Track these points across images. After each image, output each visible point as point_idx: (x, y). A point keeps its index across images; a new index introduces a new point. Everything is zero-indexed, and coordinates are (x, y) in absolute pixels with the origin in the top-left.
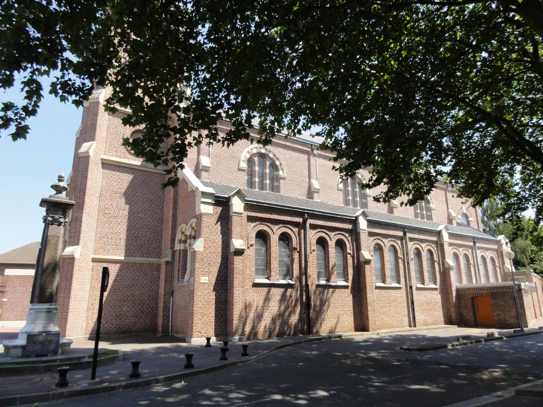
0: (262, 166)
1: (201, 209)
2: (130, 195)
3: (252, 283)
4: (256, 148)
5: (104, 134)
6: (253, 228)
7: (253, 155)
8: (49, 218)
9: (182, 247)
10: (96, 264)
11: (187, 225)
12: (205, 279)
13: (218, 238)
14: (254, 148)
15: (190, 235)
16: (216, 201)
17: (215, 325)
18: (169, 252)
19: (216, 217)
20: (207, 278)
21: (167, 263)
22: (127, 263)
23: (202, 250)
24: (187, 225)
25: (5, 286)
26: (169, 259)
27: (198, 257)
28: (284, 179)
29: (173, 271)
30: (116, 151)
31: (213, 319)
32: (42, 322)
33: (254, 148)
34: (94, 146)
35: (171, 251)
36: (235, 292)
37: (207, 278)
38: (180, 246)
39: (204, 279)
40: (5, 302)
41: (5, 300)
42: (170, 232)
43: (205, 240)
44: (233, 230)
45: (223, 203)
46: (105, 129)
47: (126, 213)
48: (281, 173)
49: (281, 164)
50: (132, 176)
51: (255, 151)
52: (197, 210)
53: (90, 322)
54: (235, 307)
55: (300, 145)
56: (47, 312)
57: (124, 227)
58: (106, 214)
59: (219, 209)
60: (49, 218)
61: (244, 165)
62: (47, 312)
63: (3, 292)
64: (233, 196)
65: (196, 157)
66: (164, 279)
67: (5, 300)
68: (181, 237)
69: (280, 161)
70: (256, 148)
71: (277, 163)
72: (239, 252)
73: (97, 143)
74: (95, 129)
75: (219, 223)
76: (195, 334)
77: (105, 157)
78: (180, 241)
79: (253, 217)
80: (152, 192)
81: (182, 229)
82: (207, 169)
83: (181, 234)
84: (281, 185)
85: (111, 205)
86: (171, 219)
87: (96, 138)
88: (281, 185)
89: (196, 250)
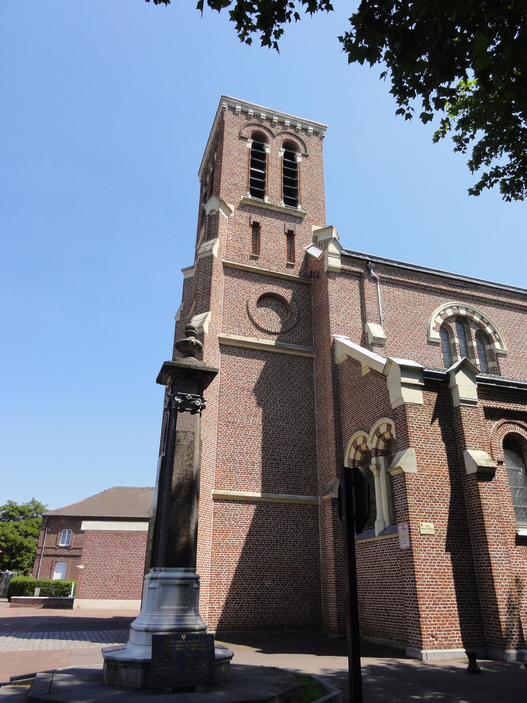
0: (465, 336)
1: (404, 395)
2: (263, 392)
3: (513, 536)
4: (451, 307)
5: (221, 302)
6: (497, 431)
7: (448, 319)
8: (177, 399)
10: (219, 505)
11: (368, 433)
12: (429, 526)
13: (440, 448)
14: (447, 308)
15: (376, 450)
16: (425, 381)
17: (461, 624)
19: (430, 410)
20: (432, 525)
22: (265, 503)
23: (416, 471)
24: (368, 433)
25: (81, 549)
27: (411, 485)
28: (504, 355)
30: (239, 326)
31: (455, 610)
32: (173, 607)
33: (447, 308)
34: (209, 319)
36: (492, 554)
39: (427, 527)
40: (82, 570)
41: (81, 567)
42: (332, 448)
43: (418, 453)
44: (467, 434)
45: (438, 385)
46: (221, 294)
47: (259, 420)
48: (497, 345)
49: (495, 332)
50: (263, 363)
51: (450, 313)
52: (392, 400)
53: (216, 606)
54: (497, 585)
55: (521, 299)
56: (180, 585)
57: (258, 443)
58: (229, 422)
59: (433, 396)
60: (177, 399)
61: (435, 335)
62: (180, 585)
63: (79, 556)
64: (456, 371)
65: (360, 325)
67: (81, 567)
68: (378, 444)
69: (492, 328)
70: (451, 307)
71: (489, 330)
72: (486, 474)
73: (212, 315)
74: (209, 294)
75: (437, 422)
76: (427, 640)
77: (223, 335)
79: (493, 409)
80: (294, 387)
81: (355, 441)
82: (382, 342)
83: (353, 450)
84: (501, 366)
85: (236, 408)
86: (331, 427)
87: (212, 306)
88: (501, 365)
89: (405, 470)
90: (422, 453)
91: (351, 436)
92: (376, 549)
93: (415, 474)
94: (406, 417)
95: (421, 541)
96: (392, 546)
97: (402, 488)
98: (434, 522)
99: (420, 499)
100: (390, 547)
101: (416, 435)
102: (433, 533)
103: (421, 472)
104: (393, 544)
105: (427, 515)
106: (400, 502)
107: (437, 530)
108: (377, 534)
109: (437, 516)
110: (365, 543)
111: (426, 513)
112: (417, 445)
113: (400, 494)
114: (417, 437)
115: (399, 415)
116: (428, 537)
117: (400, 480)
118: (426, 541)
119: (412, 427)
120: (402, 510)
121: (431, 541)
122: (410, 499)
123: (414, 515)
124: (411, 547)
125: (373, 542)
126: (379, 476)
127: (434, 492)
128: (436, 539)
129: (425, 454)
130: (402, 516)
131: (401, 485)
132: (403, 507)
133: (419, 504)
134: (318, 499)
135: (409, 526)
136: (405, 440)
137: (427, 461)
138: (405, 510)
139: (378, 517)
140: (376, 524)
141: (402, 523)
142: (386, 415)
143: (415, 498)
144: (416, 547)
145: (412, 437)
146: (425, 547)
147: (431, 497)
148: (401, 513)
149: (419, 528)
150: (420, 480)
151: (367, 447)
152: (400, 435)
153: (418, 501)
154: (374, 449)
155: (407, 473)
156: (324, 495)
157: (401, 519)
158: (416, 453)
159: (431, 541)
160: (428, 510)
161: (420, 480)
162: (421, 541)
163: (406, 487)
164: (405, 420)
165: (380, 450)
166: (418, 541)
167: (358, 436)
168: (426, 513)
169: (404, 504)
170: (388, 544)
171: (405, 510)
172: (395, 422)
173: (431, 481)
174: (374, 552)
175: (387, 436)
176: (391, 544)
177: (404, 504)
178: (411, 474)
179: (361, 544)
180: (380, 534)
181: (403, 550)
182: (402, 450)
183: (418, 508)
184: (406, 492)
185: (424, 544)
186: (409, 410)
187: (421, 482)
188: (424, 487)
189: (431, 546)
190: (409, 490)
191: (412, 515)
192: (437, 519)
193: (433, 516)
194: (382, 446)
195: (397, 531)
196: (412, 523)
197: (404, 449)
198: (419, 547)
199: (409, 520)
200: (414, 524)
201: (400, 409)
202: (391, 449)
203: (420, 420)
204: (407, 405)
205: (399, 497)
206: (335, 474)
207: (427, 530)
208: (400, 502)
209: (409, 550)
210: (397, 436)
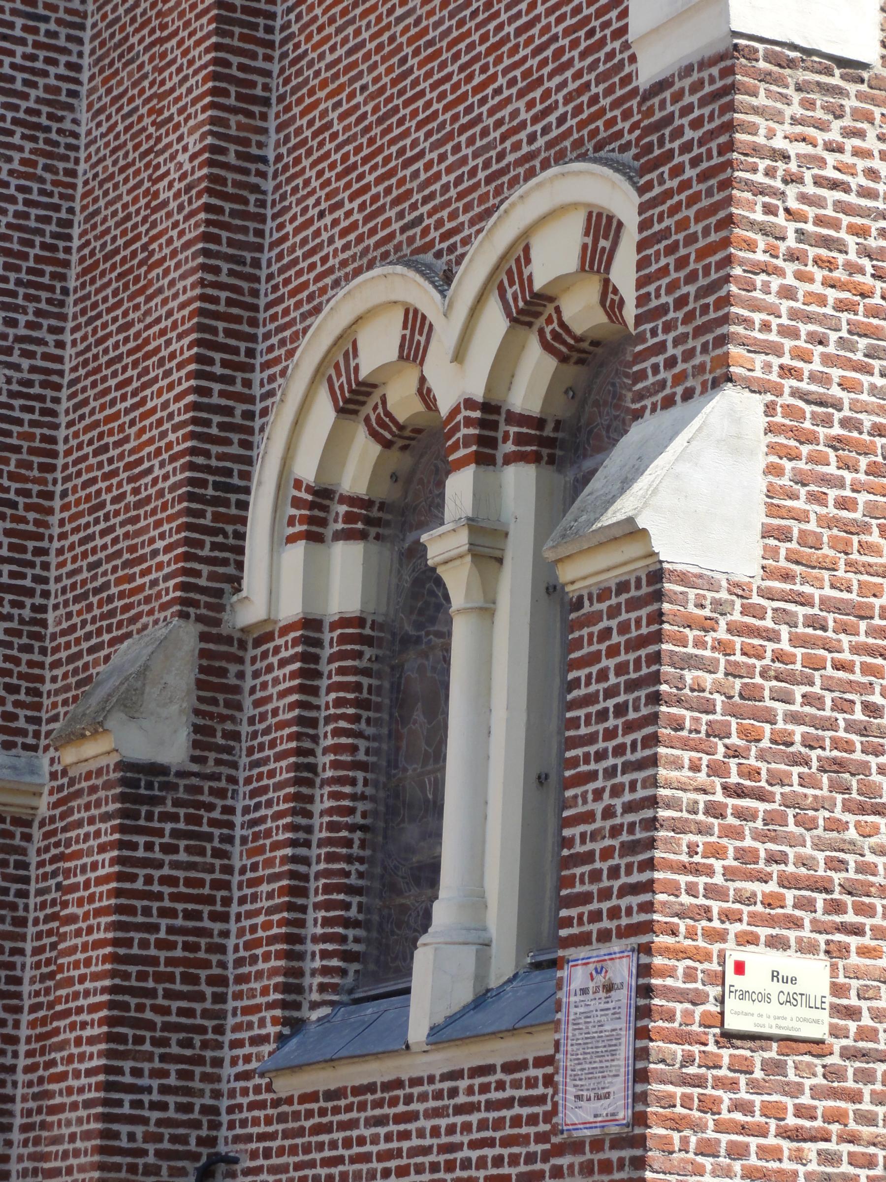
9: (346, 581)
11: (445, 280)
15: (489, 412)
18: (167, 650)
20: (814, 975)
21: (140, 783)
26: (172, 746)
27: (699, 669)
29: (207, 900)
35: (188, 636)
37: (814, 975)
38: (314, 580)
42: (170, 395)
43: (786, 435)
66: (95, 992)
68: (334, 448)
78: (316, 514)
81: (347, 345)
83: (324, 413)
86: (180, 229)
89: (672, 548)
90: (811, 439)
91: (317, 310)
92: (405, 1135)
93: (738, 589)
94: (730, 146)
95: (719, 1083)
96: (516, 1121)
97: (632, 686)
98: (836, 952)
99: (753, 774)
100: (499, 1124)
101: (787, 293)
102: (815, 1025)
103: (787, 577)
104: (525, 1102)
105: (790, 895)
106: (598, 794)
107: (852, 1013)
108: (417, 1032)
109: (860, 910)
110: (330, 1095)
111: (786, 882)
112: (786, 371)
113: (610, 734)
114: (794, 315)
115: (678, 133)
116: (772, 1054)
117: (624, 628)
118: (755, 1087)
119: (764, 230)
120: (607, 853)
121: (795, 1090)
122: (679, 775)
123: (691, 890)
124: (641, 1119)
125: (388, 1086)
126: (486, 611)
127: (863, 731)
128: (832, 1073)
129: (836, 443)
130: (606, 894)
131: (621, 669)
132: (615, 831)
133: (739, 814)
134: (33, 770)
135: (645, 970)
136: (699, 331)
137: (843, 504)
138: (630, 848)
139: (443, 913)
140: (423, 960)
141: (596, 951)
142: (595, 147)
143: (716, 770)
144: (677, 1123)
145: (756, 307)
146: (743, 1129)
147: (839, 766)
148: (596, 876)
149: (713, 991)
150: (773, 636)
151: (425, 394)
152: (672, 287)
153: (738, 792)
154: (470, 403)
155: (683, 578)
156: (74, 737)
157: (596, 916)
158: (770, 429)
159: (795, 1090)
160: (803, 862)
161: (773, 636)
162: (719, 1083)
163: (656, 678)
164: (720, 176)
165: (514, 418)
166: (699, 1082)
167: (366, 311)
168: (786, 882)
169: (629, 808)
170: (491, 1106)
171: (630, 848)
172: (641, 190)
173: (856, 649)
174: (383, 1156)
175: (581, 311)
176: (508, 1103)
177: (629, 808)
178: (713, 586)
179: (306, 1098)
180: (439, 1035)
181: (577, 1147)
182: (668, 402)
183: (731, 845)
184: (654, 718)
185: (738, 1106)
186: (761, 100)
187: (778, 657)
188: (798, 691)
189: (791, 1121)
190: (679, 702)
191: (675, 892)
192: (857, 931)
193: (836, 907)
194: (532, 384)
195: (547, 1014)
196: (667, 951)
197: (688, 395)
198: (697, 1127)
199: (647, 927)
200: (679, 954)
201: (696, 87)
202: (593, 403)
203: (835, 185)
204: (752, 55)
205: (601, 756)
206: (170, 590)
207: (774, 1008)
208: (598, 794)
209: (618, 1143)
210: (642, 300)
